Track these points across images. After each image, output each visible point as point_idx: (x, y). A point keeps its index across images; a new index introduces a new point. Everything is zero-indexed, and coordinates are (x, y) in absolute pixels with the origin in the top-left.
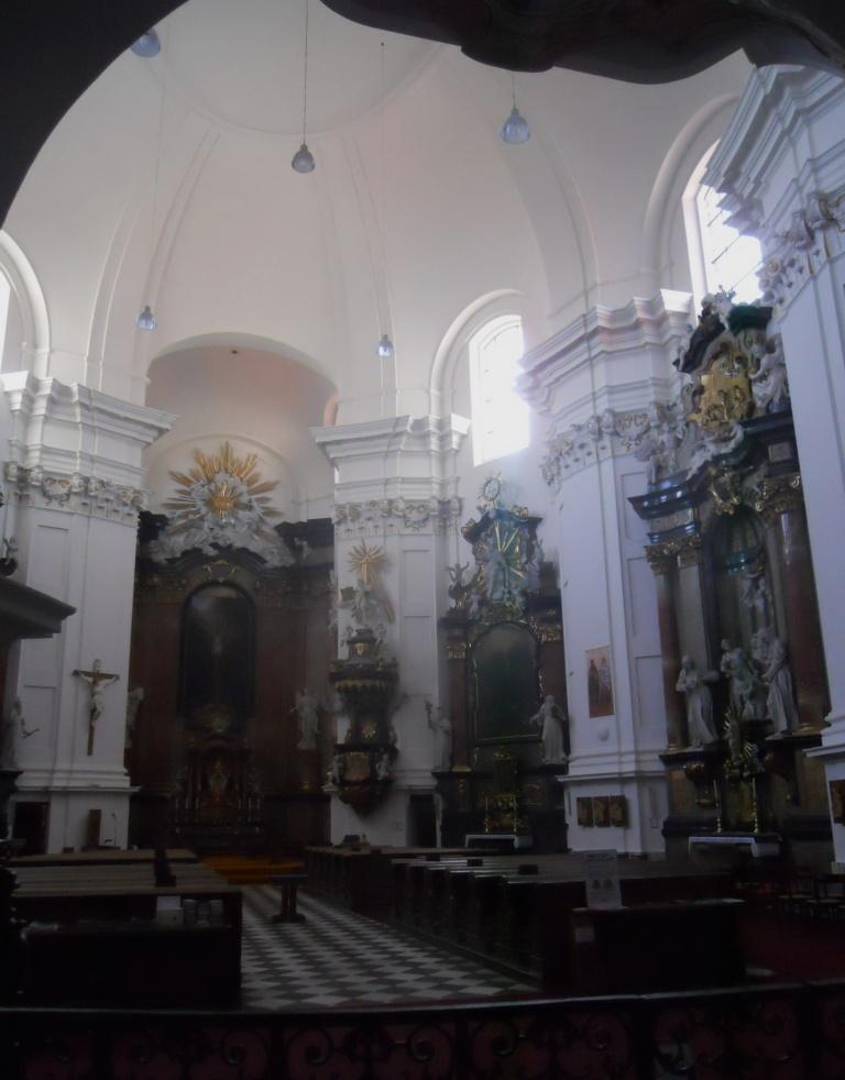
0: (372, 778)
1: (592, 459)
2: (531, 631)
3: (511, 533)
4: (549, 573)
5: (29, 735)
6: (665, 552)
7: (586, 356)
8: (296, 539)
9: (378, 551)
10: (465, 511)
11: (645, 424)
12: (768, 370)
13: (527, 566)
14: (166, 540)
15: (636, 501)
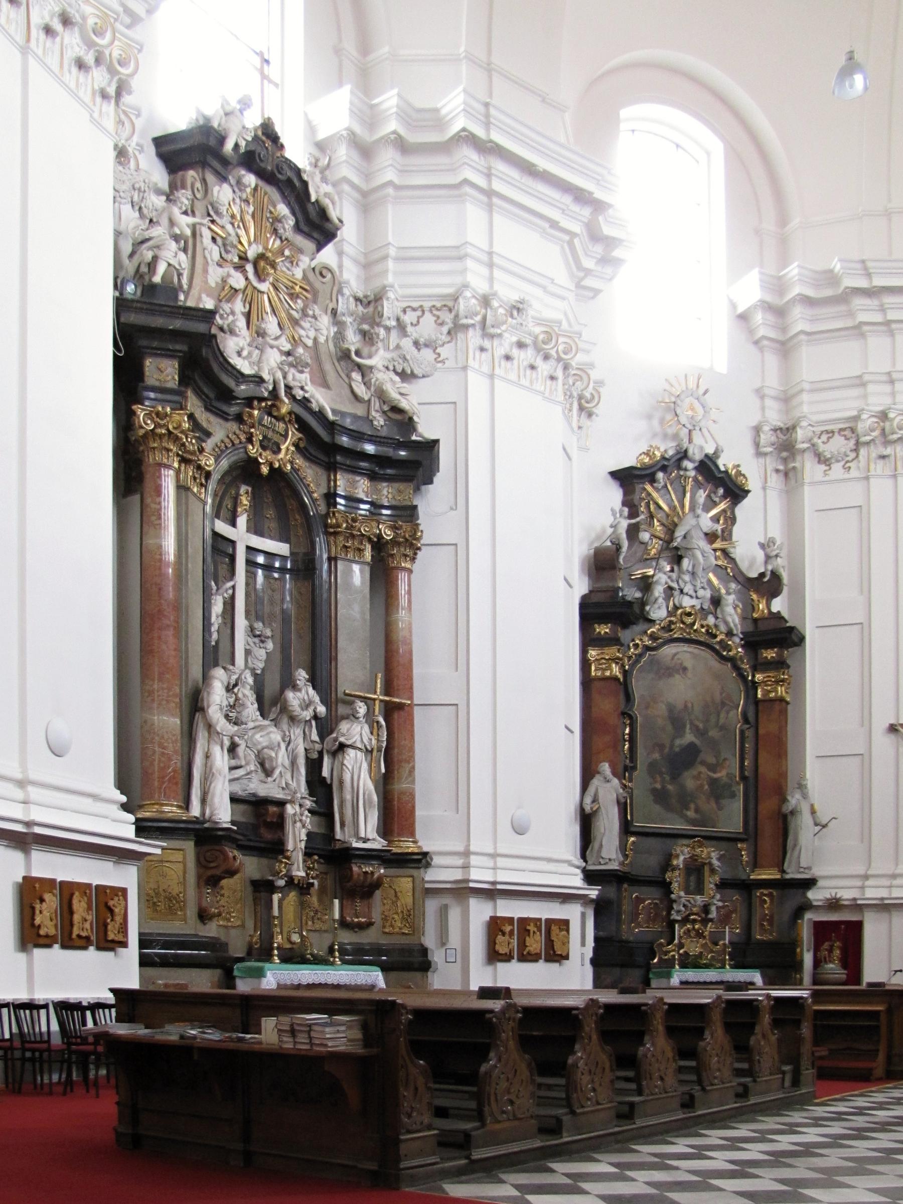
5: (824, 826)
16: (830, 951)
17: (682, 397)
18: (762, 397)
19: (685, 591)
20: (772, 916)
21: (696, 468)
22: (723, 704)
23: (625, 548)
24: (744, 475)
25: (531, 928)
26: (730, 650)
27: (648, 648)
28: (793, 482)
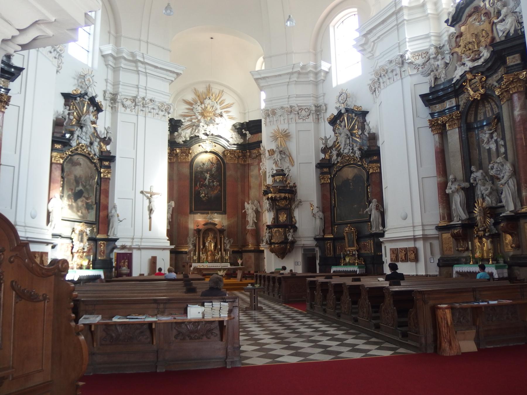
0: (285, 241)
1: (399, 77)
2: (364, 168)
3: (353, 119)
4: (373, 138)
5: (121, 221)
6: (439, 122)
7: (395, 23)
8: (243, 130)
9: (285, 131)
10: (328, 111)
11: (427, 57)
12: (506, 16)
13: (361, 136)
14: (182, 132)
15: (423, 96)
16: (124, 263)
17: (87, 75)
18: (107, 82)
19: (83, 138)
20: (104, 251)
21: (88, 99)
22: (91, 177)
23: (67, 120)
24: (102, 105)
25: (37, 255)
26: (94, 160)
27: (70, 155)
28: (114, 110)
